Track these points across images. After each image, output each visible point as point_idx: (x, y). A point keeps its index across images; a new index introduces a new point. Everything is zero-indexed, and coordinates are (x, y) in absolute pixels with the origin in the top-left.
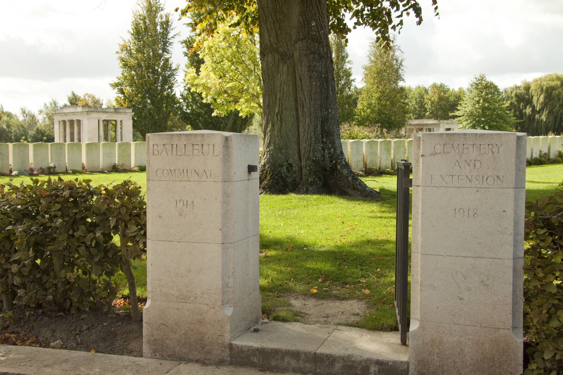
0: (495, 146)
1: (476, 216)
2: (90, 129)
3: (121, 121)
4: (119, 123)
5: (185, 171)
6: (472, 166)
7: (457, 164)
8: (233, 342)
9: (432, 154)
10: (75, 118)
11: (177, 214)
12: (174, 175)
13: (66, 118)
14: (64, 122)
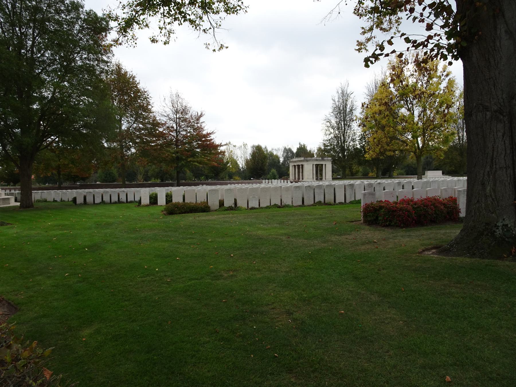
2: (309, 168)
4: (324, 166)
10: (300, 164)
13: (296, 164)
14: (295, 166)
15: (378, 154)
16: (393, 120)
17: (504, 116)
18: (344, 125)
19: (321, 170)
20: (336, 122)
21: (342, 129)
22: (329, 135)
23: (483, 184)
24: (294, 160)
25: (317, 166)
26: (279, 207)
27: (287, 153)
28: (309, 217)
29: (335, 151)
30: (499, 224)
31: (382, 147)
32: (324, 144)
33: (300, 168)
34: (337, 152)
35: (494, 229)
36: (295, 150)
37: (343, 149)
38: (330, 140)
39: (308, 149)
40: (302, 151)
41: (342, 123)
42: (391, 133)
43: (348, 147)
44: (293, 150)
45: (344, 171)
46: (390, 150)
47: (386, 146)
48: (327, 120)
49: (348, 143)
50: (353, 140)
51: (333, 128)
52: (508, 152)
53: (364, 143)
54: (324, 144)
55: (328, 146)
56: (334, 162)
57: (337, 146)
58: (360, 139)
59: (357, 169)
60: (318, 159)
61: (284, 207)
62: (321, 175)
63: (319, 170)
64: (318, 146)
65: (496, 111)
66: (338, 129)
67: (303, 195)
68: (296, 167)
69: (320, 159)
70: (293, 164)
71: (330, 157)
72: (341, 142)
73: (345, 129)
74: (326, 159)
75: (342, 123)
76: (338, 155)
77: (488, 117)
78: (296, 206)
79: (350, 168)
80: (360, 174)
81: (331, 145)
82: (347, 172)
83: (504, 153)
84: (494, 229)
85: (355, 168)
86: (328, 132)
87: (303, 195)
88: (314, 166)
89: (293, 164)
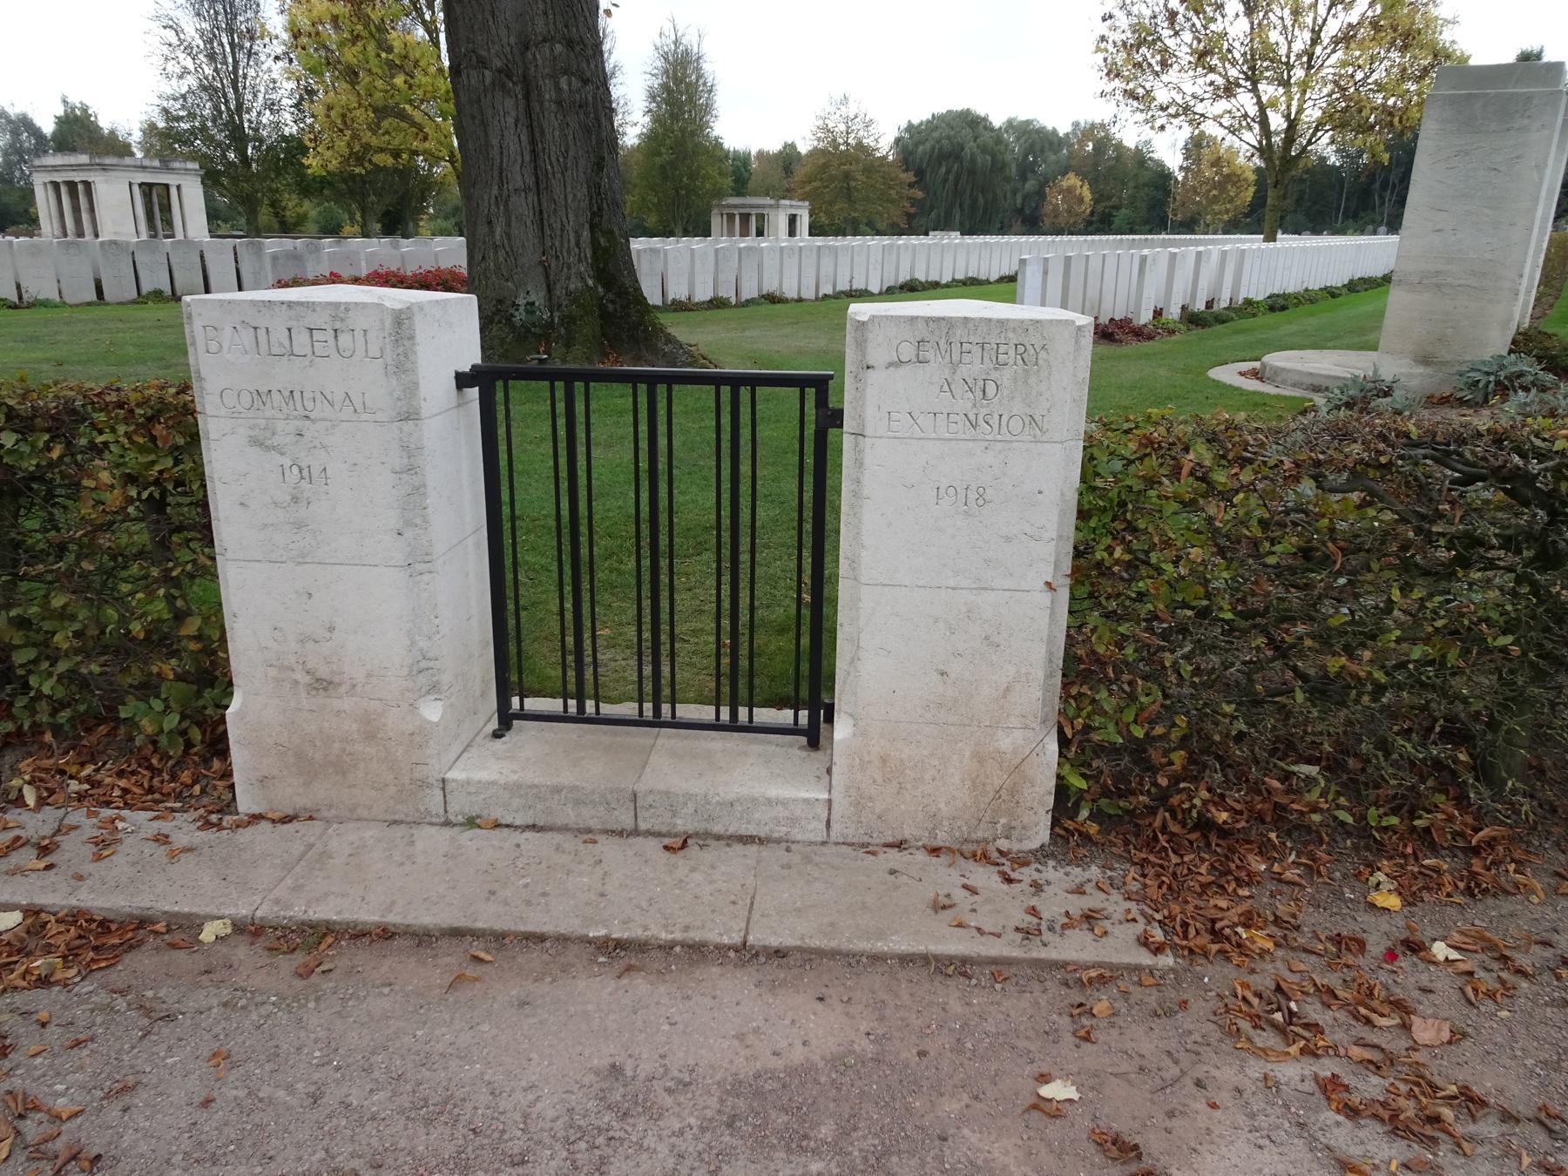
0: (1030, 348)
1: (981, 502)
2: (115, 201)
3: (178, 187)
4: (173, 192)
5: (297, 395)
6: (979, 394)
7: (946, 388)
8: (449, 776)
9: (890, 365)
10: (77, 177)
11: (288, 498)
12: (269, 405)
13: (59, 177)
14: (56, 185)
15: (346, 161)
16: (378, 55)
17: (515, 84)
18: (232, 44)
19: (166, 208)
20: (202, 33)
21: (226, 63)
22: (181, 77)
23: (490, 223)
24: (50, 160)
25: (147, 188)
26: (16, 307)
27: (15, 133)
28: (120, 325)
29: (209, 140)
30: (521, 301)
31: (355, 137)
32: (165, 111)
33: (78, 194)
34: (219, 144)
35: (512, 311)
36: (48, 127)
37: (238, 136)
38: (184, 97)
39: (105, 124)
40: (78, 131)
41: (225, 40)
42: (378, 95)
43: (256, 130)
44: (38, 122)
45: (252, 213)
46: (382, 150)
47: (367, 137)
48: (166, 22)
49: (254, 114)
50: (272, 106)
51: (189, 50)
52: (527, 158)
53: (309, 121)
54: (165, 111)
55: (179, 119)
56: (210, 179)
57: (214, 121)
58: (296, 106)
59: (301, 211)
60: (147, 163)
61: (30, 306)
62: (169, 223)
63: (157, 205)
64: (145, 117)
65: (500, 71)
66: (212, 57)
67: (96, 271)
68: (63, 189)
69: (156, 163)
70: (48, 178)
71: (194, 160)
72: (228, 108)
73: (236, 62)
74: (177, 165)
75: (225, 40)
76: (224, 156)
77: (488, 81)
78: (77, 305)
79: (272, 205)
80: (312, 227)
81: (192, 116)
82: (265, 215)
83: (519, 159)
84: (512, 311)
85: (292, 204)
86: (172, 67)
87: (96, 271)
88: (136, 189)
89: (48, 178)
